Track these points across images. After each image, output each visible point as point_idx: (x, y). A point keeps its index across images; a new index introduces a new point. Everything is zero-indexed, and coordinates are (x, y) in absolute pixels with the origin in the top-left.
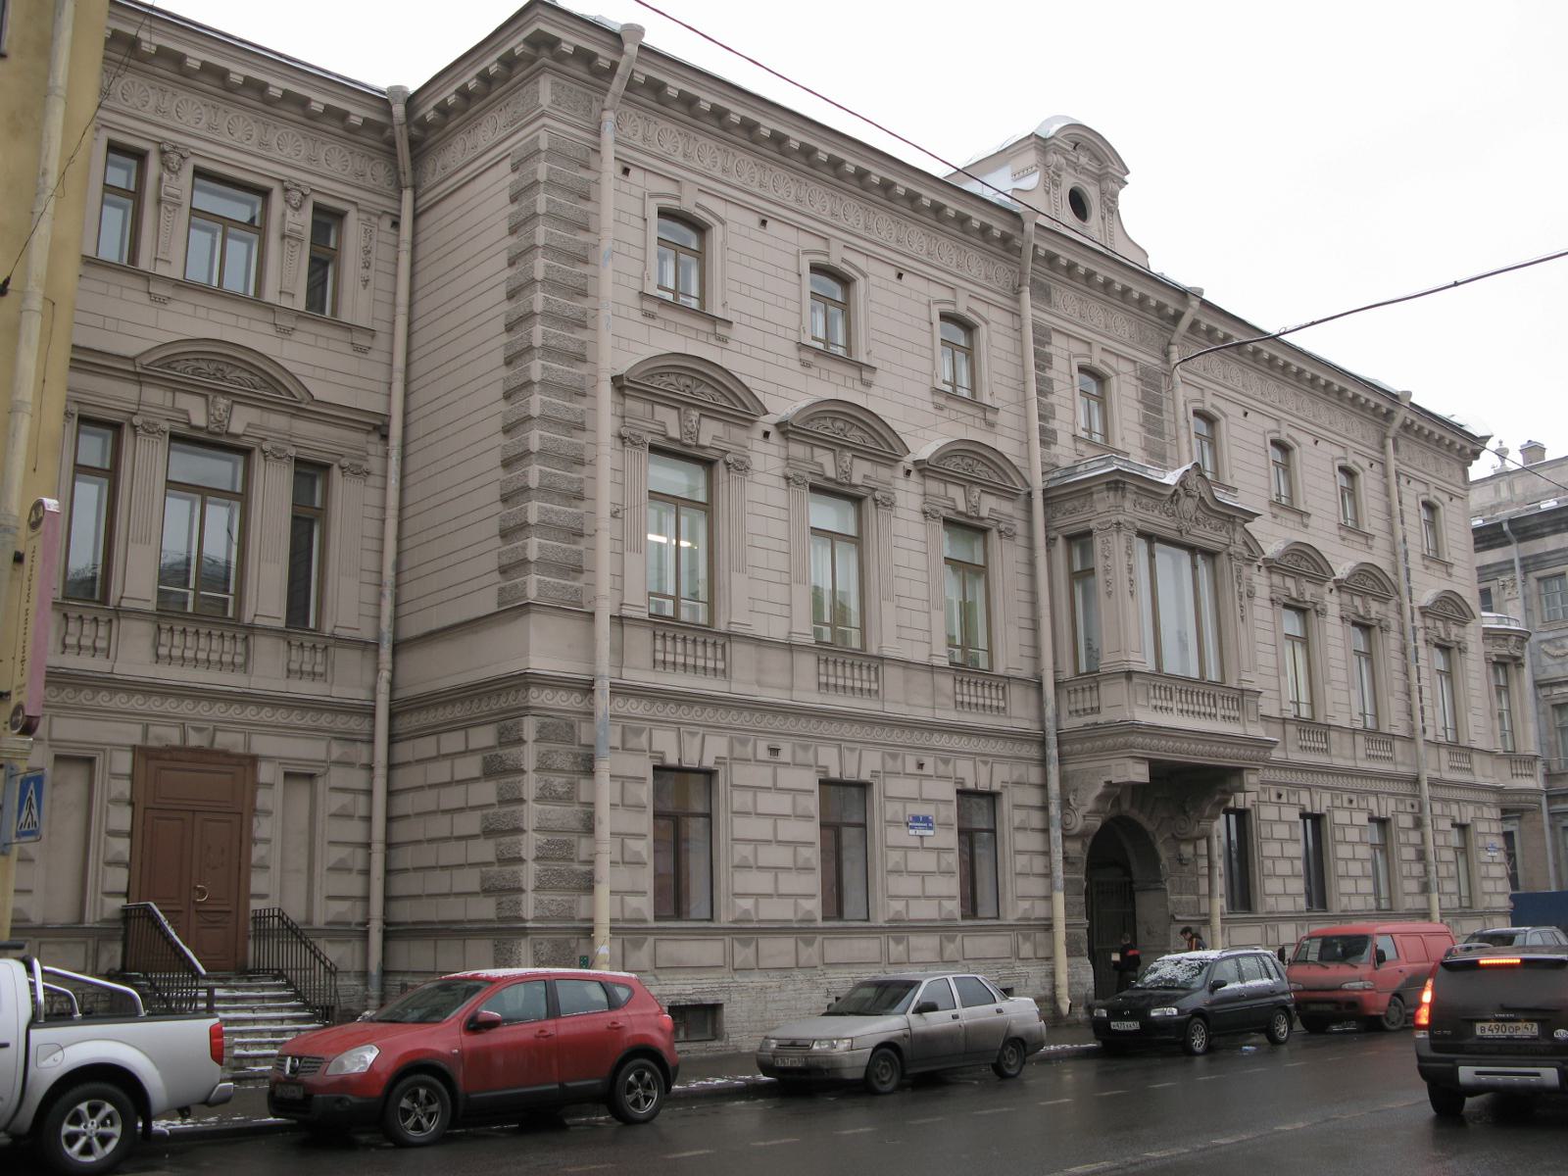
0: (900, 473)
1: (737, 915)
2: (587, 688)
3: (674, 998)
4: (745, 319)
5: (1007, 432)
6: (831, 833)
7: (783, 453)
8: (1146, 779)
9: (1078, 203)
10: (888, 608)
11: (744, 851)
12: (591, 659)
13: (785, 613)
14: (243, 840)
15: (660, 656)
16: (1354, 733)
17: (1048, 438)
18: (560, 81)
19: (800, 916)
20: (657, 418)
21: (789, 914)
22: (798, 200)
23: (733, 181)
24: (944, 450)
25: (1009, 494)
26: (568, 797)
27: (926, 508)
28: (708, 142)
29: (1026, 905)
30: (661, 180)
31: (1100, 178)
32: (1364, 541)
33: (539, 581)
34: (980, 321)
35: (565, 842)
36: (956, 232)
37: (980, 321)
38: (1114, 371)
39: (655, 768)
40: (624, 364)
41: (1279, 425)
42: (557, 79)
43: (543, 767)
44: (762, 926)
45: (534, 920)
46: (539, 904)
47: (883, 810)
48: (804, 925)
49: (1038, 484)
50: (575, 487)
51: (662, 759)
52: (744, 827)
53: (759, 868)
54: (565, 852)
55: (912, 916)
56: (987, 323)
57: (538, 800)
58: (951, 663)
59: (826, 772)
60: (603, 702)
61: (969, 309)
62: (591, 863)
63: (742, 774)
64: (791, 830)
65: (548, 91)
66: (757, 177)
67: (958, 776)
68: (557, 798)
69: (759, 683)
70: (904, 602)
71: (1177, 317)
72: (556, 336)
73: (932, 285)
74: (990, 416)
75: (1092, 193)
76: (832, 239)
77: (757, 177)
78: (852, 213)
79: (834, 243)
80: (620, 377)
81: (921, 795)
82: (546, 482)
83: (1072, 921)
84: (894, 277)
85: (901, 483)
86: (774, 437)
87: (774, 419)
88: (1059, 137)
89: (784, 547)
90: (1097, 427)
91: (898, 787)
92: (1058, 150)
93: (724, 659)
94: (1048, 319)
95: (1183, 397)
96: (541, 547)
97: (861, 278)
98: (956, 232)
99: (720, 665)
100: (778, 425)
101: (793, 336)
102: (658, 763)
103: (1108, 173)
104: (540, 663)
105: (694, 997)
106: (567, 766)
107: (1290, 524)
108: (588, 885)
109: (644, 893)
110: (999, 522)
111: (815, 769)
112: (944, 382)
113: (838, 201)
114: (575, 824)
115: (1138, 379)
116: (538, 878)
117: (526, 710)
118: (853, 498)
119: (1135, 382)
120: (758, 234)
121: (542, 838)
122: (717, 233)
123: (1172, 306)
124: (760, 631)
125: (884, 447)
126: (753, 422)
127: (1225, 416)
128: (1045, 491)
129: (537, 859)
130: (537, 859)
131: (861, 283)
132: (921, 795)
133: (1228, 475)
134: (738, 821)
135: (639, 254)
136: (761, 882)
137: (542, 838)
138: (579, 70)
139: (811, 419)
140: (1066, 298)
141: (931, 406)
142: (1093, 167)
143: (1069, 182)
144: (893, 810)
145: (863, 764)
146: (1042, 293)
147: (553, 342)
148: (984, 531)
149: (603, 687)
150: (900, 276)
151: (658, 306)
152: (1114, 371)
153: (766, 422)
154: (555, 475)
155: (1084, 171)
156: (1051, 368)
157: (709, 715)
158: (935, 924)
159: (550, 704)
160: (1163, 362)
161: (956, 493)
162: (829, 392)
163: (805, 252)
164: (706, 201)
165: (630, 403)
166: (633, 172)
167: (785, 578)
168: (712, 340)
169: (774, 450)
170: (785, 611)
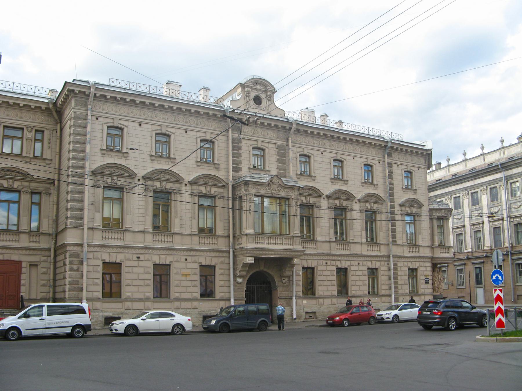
0: (184, 185)
1: (126, 297)
2: (82, 245)
3: (106, 316)
4: (419, 189)
5: (223, 170)
6: (158, 278)
7: (190, 189)
8: (253, 262)
9: (258, 100)
10: (351, 232)
11: (128, 281)
12: (83, 239)
13: (190, 227)
14: (19, 280)
15: (337, 248)
16: (362, 244)
17: (236, 169)
18: (78, 99)
19: (193, 297)
20: (335, 202)
21: (190, 297)
22: (175, 121)
23: (131, 116)
24: (196, 178)
25: (223, 187)
26: (78, 270)
27: (329, 206)
28: (334, 142)
29: (222, 294)
30: (253, 141)
31: (266, 91)
32: (374, 186)
33: (70, 222)
34: (413, 171)
35: (77, 281)
36: (142, 106)
37: (413, 171)
38: (267, 147)
39: (154, 264)
40: (94, 167)
41: (407, 167)
42: (76, 99)
43: (71, 263)
44: (94, 299)
45: (68, 298)
46: (69, 294)
47: (380, 273)
48: (194, 299)
49: (231, 184)
50: (80, 199)
51: (201, 264)
52: (128, 276)
53: (324, 286)
54: (77, 283)
55: (182, 297)
56: (414, 171)
57: (69, 271)
58: (408, 243)
59: (304, 266)
60: (85, 248)
61: (410, 169)
62: (82, 285)
63: (320, 268)
64: (362, 278)
65: (74, 102)
66: (206, 124)
67: (200, 262)
68: (75, 271)
69: (134, 242)
70: (424, 234)
71: (290, 129)
72: (75, 163)
73: (402, 166)
74: (415, 191)
75: (263, 96)
76: (162, 126)
77: (173, 118)
78: (342, 146)
79: (305, 149)
80: (359, 199)
81: (138, 265)
82: (72, 198)
83: (235, 299)
84: (184, 133)
85: (354, 204)
86: (188, 185)
87: (357, 199)
88: (248, 83)
89: (144, 207)
90: (410, 184)
91: (177, 265)
92: (248, 87)
93: (316, 246)
94: (391, 161)
95: (293, 153)
96: (71, 214)
97: (345, 161)
98: (142, 106)
99: (216, 243)
100: (143, 177)
101: (149, 153)
102: (104, 262)
103: (267, 90)
104: (69, 240)
105: (112, 316)
106: (77, 263)
107: (306, 180)
108: (81, 290)
109: (335, 291)
110: (316, 204)
111: (151, 262)
112: (405, 185)
113: (209, 122)
114: (79, 276)
115: (276, 148)
116: (69, 289)
117: (66, 251)
118: (121, 189)
119: (275, 149)
120: (321, 156)
121: (70, 279)
122: (345, 162)
123: (288, 126)
124: (136, 228)
125: (350, 197)
126: (181, 182)
127: (345, 160)
128: (233, 185)
129: (69, 284)
130: (69, 284)
131: (312, 157)
132: (138, 265)
133: (414, 186)
134: (352, 277)
135: (100, 139)
136: (357, 288)
137: (70, 279)
138: (82, 96)
139: (365, 197)
140: (395, 155)
141: (196, 166)
142: (263, 89)
143: (253, 94)
144: (382, 273)
145: (416, 265)
146: (390, 155)
147: (74, 165)
148: (215, 197)
149: (85, 245)
150: (186, 132)
151: (406, 189)
152: (267, 147)
153: (324, 196)
154: (75, 196)
155: (259, 90)
156: (241, 150)
157: (119, 250)
158: (91, 299)
159: (73, 249)
160: (286, 142)
161: (368, 205)
162: (206, 172)
163: (332, 158)
164: (372, 161)
165: (361, 203)
166: (99, 118)
167: (144, 215)
168: (123, 158)
169: (188, 188)
170: (144, 223)
